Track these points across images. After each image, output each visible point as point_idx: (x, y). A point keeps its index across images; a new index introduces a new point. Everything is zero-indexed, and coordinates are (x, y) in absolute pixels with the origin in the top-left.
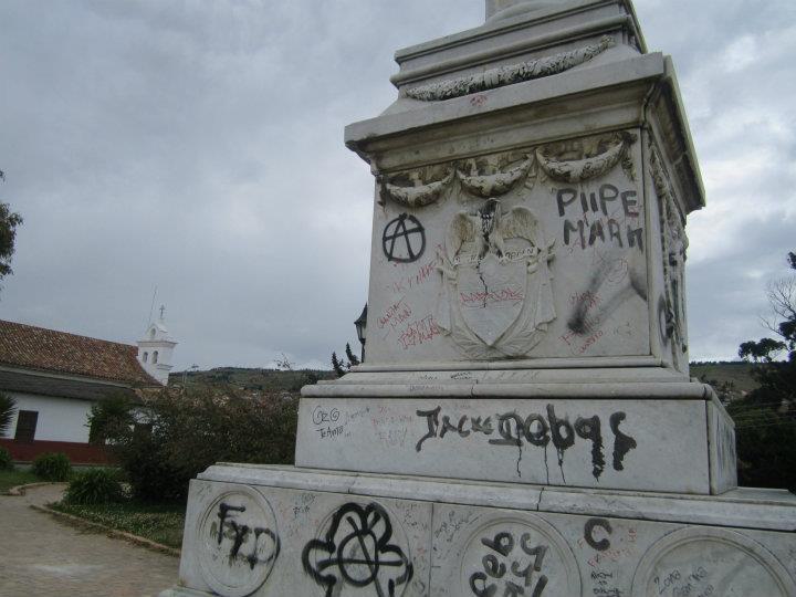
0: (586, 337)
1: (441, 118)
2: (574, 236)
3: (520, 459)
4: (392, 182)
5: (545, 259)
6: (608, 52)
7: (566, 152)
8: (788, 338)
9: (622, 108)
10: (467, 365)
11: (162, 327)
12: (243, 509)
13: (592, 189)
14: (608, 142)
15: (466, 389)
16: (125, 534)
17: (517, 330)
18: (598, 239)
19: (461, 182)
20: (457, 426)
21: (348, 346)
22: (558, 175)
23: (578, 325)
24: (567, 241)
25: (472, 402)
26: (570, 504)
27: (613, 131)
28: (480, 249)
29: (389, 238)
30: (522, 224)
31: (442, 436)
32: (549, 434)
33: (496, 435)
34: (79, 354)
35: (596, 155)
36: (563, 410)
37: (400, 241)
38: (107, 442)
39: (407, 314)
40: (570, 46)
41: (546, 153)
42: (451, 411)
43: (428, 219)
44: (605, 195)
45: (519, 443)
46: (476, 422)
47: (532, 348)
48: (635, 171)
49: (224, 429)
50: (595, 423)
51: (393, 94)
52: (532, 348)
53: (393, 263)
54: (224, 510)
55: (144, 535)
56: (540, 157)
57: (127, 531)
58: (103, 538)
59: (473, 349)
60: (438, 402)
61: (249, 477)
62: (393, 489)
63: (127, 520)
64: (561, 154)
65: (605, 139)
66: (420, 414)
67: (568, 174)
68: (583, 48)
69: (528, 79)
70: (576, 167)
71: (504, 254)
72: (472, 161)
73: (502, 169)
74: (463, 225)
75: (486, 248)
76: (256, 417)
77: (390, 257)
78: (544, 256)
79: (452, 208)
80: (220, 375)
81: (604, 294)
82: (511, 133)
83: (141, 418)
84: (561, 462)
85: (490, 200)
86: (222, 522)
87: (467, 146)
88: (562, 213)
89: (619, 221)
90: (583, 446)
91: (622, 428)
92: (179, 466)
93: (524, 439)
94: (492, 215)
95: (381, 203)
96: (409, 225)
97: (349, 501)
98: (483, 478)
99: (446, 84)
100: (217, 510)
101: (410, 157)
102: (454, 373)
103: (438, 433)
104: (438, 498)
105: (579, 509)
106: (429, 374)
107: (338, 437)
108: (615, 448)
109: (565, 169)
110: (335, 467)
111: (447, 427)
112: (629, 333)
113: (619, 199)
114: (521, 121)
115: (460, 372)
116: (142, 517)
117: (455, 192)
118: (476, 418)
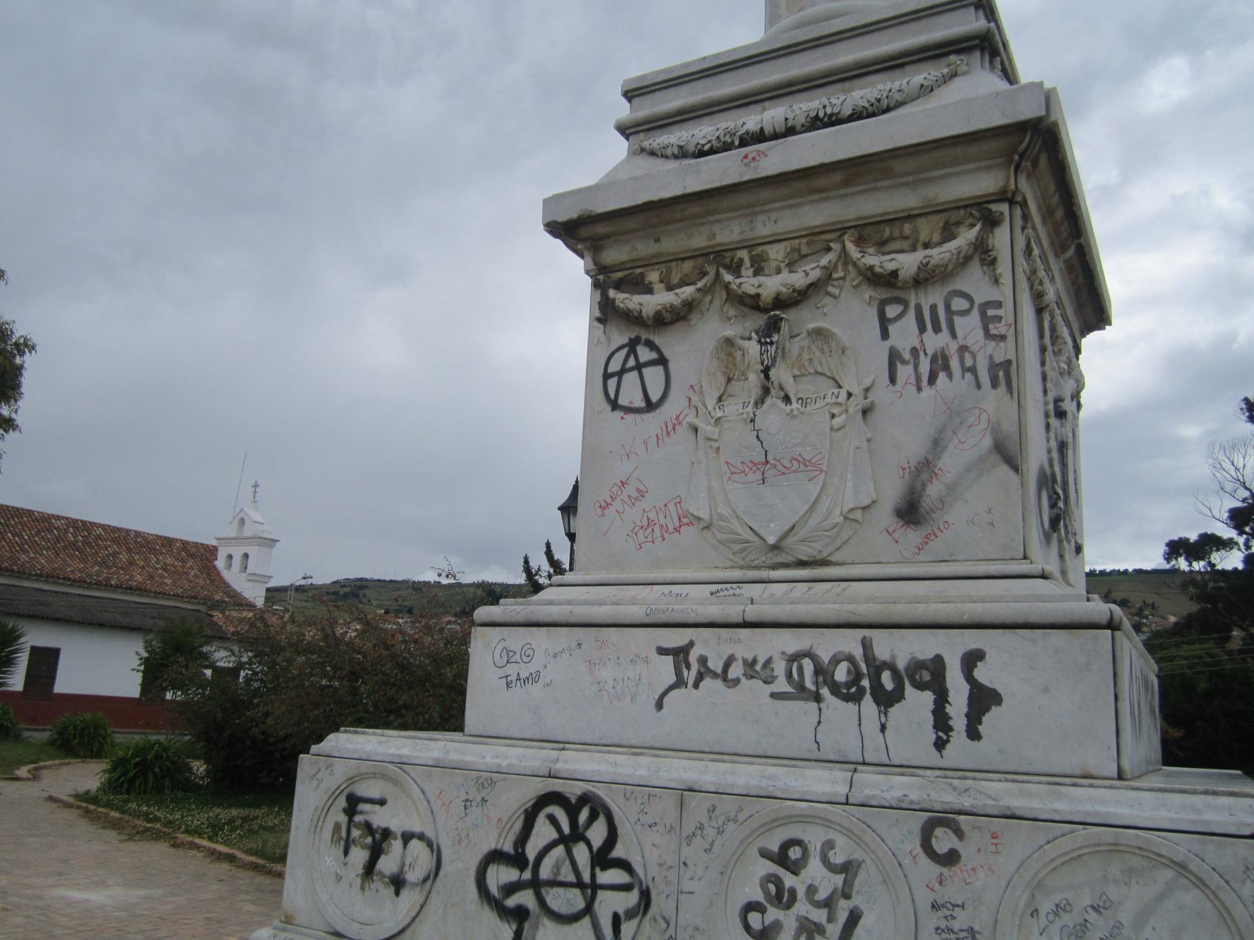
0: (924, 531)
1: (694, 184)
2: (904, 372)
3: (819, 722)
4: (618, 286)
6: (958, 82)
7: (892, 238)
8: (1241, 533)
9: (979, 169)
10: (736, 574)
11: (256, 516)
12: (382, 802)
13: (933, 297)
14: (958, 224)
15: (733, 612)
16: (198, 841)
17: (814, 520)
18: (942, 376)
19: (727, 286)
20: (719, 671)
21: (548, 545)
22: (880, 276)
23: (910, 512)
24: (893, 380)
25: (744, 633)
26: (898, 794)
27: (965, 207)
28: (756, 392)
29: (613, 375)
30: (823, 352)
31: (696, 686)
32: (865, 683)
33: (782, 685)
35: (940, 244)
36: (888, 646)
37: (631, 379)
38: (169, 696)
39: (642, 494)
40: (897, 73)
41: (860, 241)
42: (710, 646)
43: (673, 344)
44: (954, 308)
45: (818, 698)
46: (750, 664)
48: (999, 270)
49: (353, 676)
50: (937, 666)
51: (621, 146)
53: (618, 414)
54: (353, 803)
55: (227, 843)
56: (850, 247)
57: (200, 836)
58: (163, 847)
59: (744, 550)
60: (689, 633)
61: (392, 751)
63: (201, 818)
64: (883, 243)
65: (953, 220)
66: (662, 651)
67: (894, 274)
70: (907, 263)
72: (743, 254)
73: (791, 266)
75: (766, 391)
77: (615, 405)
78: (858, 403)
79: (712, 327)
80: (347, 590)
81: (951, 463)
82: (805, 209)
83: (222, 657)
84: (883, 728)
85: (771, 315)
86: (350, 821)
87: (737, 230)
88: (885, 335)
89: (975, 348)
90: (919, 702)
91: (981, 673)
93: (825, 692)
95: (599, 320)
96: (645, 354)
97: (549, 789)
99: (703, 132)
100: (342, 803)
101: (645, 248)
102: (714, 587)
103: (691, 682)
104: (690, 785)
105: (912, 802)
107: (535, 690)
108: (969, 705)
109: (890, 266)
113: (975, 314)
117: (717, 303)
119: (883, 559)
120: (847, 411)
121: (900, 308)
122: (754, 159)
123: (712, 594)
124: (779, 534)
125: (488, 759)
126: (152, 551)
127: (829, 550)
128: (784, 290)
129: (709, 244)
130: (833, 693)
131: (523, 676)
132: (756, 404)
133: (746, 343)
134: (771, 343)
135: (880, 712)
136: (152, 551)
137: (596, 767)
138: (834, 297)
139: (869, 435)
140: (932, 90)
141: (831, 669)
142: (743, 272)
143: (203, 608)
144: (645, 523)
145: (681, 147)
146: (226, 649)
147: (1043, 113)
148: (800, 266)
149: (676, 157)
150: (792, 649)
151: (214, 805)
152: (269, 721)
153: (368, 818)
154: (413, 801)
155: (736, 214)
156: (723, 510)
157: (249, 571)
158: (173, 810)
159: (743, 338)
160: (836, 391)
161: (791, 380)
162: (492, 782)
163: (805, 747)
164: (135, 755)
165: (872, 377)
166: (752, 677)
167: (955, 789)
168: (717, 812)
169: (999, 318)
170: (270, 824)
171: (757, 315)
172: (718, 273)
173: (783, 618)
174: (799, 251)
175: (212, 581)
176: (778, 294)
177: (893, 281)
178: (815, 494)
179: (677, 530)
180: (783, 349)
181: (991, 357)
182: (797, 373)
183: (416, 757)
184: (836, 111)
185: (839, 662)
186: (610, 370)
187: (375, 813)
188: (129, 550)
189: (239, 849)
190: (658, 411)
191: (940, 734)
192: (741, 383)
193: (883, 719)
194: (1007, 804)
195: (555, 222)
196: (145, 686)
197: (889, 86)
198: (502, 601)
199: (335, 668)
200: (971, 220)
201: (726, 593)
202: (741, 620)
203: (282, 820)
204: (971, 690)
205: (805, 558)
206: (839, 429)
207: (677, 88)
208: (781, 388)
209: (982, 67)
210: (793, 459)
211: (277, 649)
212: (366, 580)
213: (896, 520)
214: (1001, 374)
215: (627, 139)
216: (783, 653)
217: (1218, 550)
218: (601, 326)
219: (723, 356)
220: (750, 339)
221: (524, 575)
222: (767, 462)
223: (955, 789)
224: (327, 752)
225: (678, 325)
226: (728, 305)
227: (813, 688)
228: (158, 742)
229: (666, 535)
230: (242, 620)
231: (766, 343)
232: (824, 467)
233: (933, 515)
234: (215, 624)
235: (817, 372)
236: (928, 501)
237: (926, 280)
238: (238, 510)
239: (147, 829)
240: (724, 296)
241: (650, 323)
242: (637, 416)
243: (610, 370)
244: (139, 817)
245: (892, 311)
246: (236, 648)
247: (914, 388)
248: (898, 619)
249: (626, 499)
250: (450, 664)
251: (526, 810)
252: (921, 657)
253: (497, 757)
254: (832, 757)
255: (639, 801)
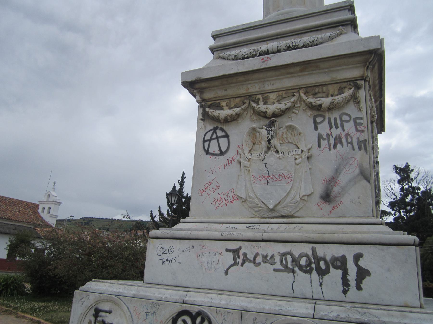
0: (332, 205)
1: (242, 69)
2: (324, 143)
3: (294, 281)
4: (210, 107)
5: (307, 156)
6: (343, 36)
7: (319, 92)
8: (393, 210)
9: (353, 68)
10: (256, 220)
11: (54, 194)
12: (110, 312)
13: (335, 115)
14: (345, 88)
15: (258, 235)
16: (26, 315)
17: (288, 200)
18: (339, 145)
19: (253, 108)
20: (252, 259)
21: (160, 208)
22: (314, 106)
23: (327, 197)
24: (319, 146)
25: (263, 244)
26: (335, 314)
27: (347, 82)
28: (265, 149)
29: (207, 141)
30: (291, 134)
31: (242, 265)
32: (313, 266)
33: (278, 266)
34: (4, 207)
35: (338, 95)
36: (321, 251)
37: (214, 143)
38: (17, 259)
39: (218, 187)
40: (319, 32)
41: (306, 93)
42: (248, 249)
43: (231, 129)
44: (343, 119)
45: (293, 272)
46: (265, 257)
47: (298, 211)
48: (361, 106)
49: (90, 254)
50: (343, 259)
51: (211, 56)
52: (298, 211)
53: (209, 156)
54: (97, 312)
55: (37, 316)
56: (302, 95)
57: (27, 313)
58: (12, 317)
59: (259, 211)
60: (239, 244)
61: (115, 290)
62: (213, 301)
63: (28, 306)
64: (315, 94)
65: (342, 86)
66: (228, 251)
67: (320, 105)
68: (328, 34)
69: (295, 49)
70: (326, 101)
71: (280, 153)
72: (260, 96)
73: (279, 101)
74: (254, 134)
75: (269, 149)
76: (115, 251)
77: (207, 152)
78: (305, 155)
79: (247, 124)
80: (86, 221)
81: (343, 179)
82: (284, 80)
83: (39, 245)
84: (321, 284)
85: (271, 119)
86: (96, 320)
87: (257, 87)
88: (316, 129)
89: (352, 135)
90: (335, 274)
91: (361, 263)
92: (62, 275)
93: (296, 269)
94: (273, 128)
95: (202, 120)
96: (220, 133)
97: (184, 309)
98: (269, 293)
99: (245, 51)
100: (92, 312)
101: (221, 93)
102: (248, 225)
103: (240, 264)
104: (245, 308)
105: (342, 318)
106: (232, 225)
107: (174, 265)
108: (357, 276)
109: (319, 103)
110: (170, 283)
111: (246, 260)
112: (359, 203)
113: (352, 122)
114: (292, 73)
115: (252, 225)
116: (36, 304)
117: (249, 115)
118: (265, 255)
119: (315, 216)
120: (301, 157)
121: (322, 119)
122: (266, 60)
123: (247, 228)
124: (274, 204)
125: (156, 295)
126: (14, 205)
127: (294, 211)
128: (277, 110)
129: (246, 92)
130: (300, 270)
131: (169, 259)
132: (265, 154)
133: (261, 130)
134: (271, 130)
135: (319, 278)
136: (14, 205)
137: (203, 300)
138: (296, 114)
139: (310, 167)
140: (333, 39)
141: (299, 260)
142: (260, 103)
143: (32, 227)
144: (219, 199)
145: (235, 56)
146: (41, 242)
147: (380, 47)
148: (282, 102)
149: (233, 60)
150: (282, 251)
151: (33, 301)
152: (56, 270)
153: (104, 319)
154: (124, 312)
155: (257, 81)
156: (251, 195)
157: (50, 214)
158: (17, 303)
159: (259, 128)
160: (297, 150)
161: (279, 145)
162: (159, 305)
163: (288, 291)
164: (3, 282)
165: (311, 145)
166: (266, 262)
167: (360, 313)
168: (257, 321)
169: (361, 124)
170: (54, 309)
171: (265, 119)
172: (250, 103)
173: (279, 238)
174: (282, 96)
175: (37, 217)
176: (274, 112)
177: (319, 108)
178: (289, 189)
179: (232, 202)
180: (276, 133)
181: (358, 138)
182: (282, 142)
183: (125, 293)
184: (297, 44)
185: (302, 257)
186: (206, 139)
187: (107, 316)
188: (6, 205)
189: (42, 319)
190: (225, 155)
191: (345, 287)
192: (258, 145)
193: (321, 281)
194: (384, 320)
195: (186, 81)
196: (9, 255)
197: (317, 36)
198: (160, 228)
199: (83, 251)
200: (350, 86)
201: (253, 227)
202: (261, 239)
203: (59, 307)
204: (357, 270)
205: (284, 215)
206: (299, 164)
207: (233, 35)
208: (275, 148)
209: (351, 31)
210: (280, 175)
211: (60, 243)
212: (93, 218)
213: (321, 200)
214: (363, 145)
215: (213, 53)
216: (279, 253)
217: (386, 216)
218: (202, 122)
219: (251, 135)
220: (262, 128)
221: (150, 218)
222: (269, 176)
223: (360, 313)
224: (87, 290)
225: (233, 122)
226: (253, 115)
227: (291, 267)
228: (13, 277)
229: (227, 204)
230: (48, 231)
231: (269, 130)
232: (293, 179)
233: (336, 199)
234: (37, 232)
235: (289, 142)
236: (334, 193)
237: (333, 108)
238: (48, 191)
239: (6, 310)
240: (252, 112)
241: (222, 121)
242: (216, 157)
243: (206, 139)
244: (3, 305)
245: (319, 120)
246: (45, 242)
247: (328, 149)
248: (326, 240)
249: (211, 189)
250: (127, 250)
251: (173, 318)
252: (337, 256)
253: (160, 294)
254: (299, 296)
255: (223, 315)
